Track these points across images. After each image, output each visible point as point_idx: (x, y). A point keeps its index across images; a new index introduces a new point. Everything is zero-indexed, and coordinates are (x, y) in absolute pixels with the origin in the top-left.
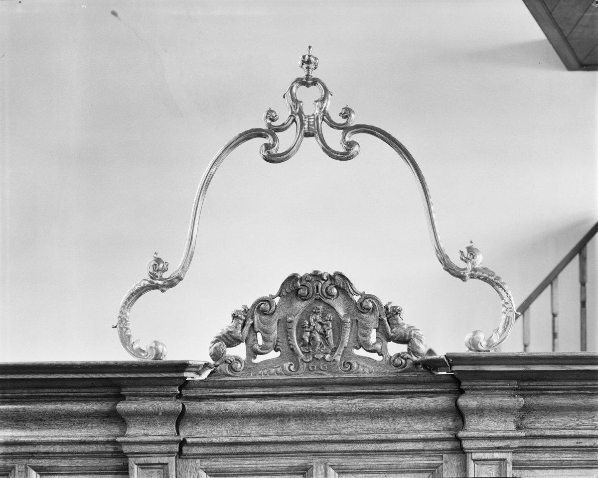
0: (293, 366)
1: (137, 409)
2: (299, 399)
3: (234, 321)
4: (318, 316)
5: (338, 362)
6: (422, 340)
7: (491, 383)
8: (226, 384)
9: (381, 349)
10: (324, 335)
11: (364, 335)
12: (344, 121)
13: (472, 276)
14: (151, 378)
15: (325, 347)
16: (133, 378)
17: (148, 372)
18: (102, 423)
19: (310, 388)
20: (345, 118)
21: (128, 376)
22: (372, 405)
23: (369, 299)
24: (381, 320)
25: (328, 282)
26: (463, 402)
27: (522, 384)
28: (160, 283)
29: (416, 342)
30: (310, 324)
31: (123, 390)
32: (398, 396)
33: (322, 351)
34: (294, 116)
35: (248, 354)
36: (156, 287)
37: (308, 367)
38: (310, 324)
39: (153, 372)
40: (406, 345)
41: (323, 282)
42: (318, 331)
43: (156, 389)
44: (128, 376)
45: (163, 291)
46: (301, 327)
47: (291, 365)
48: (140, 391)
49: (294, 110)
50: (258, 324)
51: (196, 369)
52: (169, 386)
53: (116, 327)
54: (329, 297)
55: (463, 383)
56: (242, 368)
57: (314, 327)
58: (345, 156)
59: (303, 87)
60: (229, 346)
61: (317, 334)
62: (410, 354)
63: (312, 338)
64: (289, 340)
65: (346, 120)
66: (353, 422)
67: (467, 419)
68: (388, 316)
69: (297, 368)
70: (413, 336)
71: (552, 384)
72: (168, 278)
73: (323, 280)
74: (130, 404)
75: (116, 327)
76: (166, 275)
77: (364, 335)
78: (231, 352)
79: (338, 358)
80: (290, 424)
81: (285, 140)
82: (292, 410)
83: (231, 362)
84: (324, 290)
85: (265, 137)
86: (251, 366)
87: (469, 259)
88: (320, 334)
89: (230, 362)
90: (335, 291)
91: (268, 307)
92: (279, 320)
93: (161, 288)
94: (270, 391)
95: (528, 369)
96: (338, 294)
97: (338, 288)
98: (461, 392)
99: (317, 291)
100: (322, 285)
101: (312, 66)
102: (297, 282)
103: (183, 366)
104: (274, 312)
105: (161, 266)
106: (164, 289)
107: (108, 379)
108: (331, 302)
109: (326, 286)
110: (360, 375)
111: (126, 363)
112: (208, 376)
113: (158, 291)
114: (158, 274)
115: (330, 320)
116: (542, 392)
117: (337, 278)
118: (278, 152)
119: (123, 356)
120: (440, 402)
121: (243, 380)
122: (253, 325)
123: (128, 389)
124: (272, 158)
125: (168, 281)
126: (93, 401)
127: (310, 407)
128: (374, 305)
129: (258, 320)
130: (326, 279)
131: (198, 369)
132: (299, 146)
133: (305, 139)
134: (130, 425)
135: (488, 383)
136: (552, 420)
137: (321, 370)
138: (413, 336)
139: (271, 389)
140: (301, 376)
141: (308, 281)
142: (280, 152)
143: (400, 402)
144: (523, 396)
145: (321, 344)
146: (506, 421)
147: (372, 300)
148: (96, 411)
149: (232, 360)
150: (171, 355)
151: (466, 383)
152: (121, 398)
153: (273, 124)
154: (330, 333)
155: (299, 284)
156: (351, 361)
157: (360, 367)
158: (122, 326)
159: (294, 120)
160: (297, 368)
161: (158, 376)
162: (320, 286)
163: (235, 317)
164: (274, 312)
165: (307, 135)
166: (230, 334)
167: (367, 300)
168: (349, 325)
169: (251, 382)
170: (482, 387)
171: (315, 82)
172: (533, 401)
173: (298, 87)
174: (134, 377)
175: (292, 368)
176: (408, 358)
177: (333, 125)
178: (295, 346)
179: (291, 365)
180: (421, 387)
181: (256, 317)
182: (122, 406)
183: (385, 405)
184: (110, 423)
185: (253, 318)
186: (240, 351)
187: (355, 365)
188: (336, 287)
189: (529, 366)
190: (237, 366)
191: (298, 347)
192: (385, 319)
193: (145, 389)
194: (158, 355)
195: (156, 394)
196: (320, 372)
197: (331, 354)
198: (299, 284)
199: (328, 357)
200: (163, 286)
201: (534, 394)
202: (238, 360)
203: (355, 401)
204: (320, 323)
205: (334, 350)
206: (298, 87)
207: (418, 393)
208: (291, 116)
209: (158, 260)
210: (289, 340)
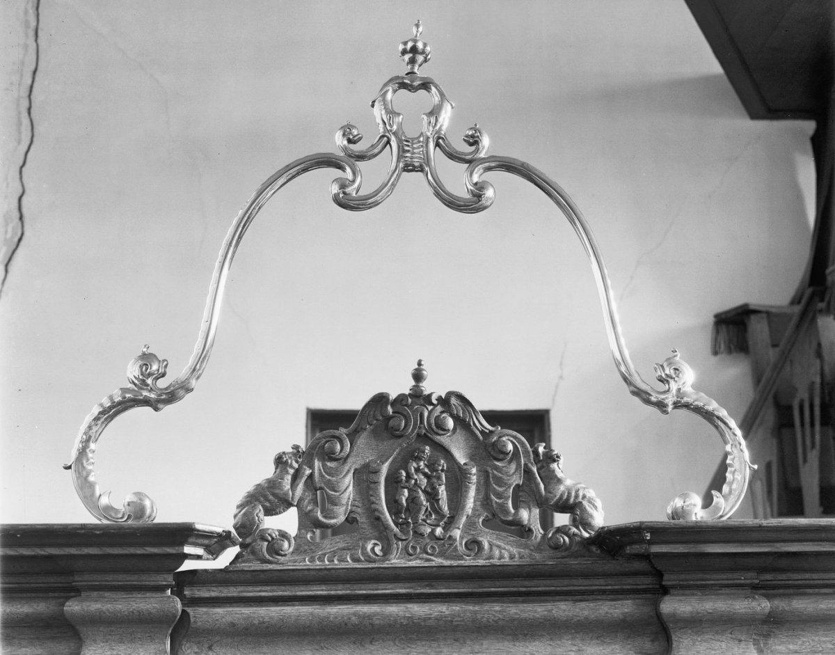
0: (380, 547)
1: (101, 612)
2: (591, 238)
3: (278, 470)
4: (422, 463)
5: (455, 540)
6: (596, 504)
7: (715, 576)
8: (262, 576)
9: (529, 520)
10: (432, 496)
11: (499, 496)
12: (467, 149)
13: (677, 405)
14: (126, 555)
15: (433, 517)
16: (95, 555)
17: (121, 545)
18: (37, 638)
19: (409, 585)
20: (471, 144)
21: (86, 551)
22: (516, 614)
23: (507, 438)
24: (528, 472)
25: (439, 408)
26: (671, 606)
27: (762, 578)
28: (153, 396)
29: (588, 508)
30: (409, 477)
31: (77, 578)
32: (557, 598)
33: (428, 521)
34: (388, 138)
35: (301, 526)
36: (146, 402)
37: (406, 548)
38: (409, 477)
39: (131, 545)
40: (568, 515)
41: (430, 408)
42: (423, 487)
43: (136, 577)
44: (86, 551)
45: (156, 409)
46: (393, 482)
47: (376, 544)
48: (108, 581)
49: (389, 128)
50: (321, 475)
51: (206, 542)
52: (159, 571)
53: (70, 467)
54: (443, 432)
55: (666, 577)
56: (291, 550)
57: (416, 480)
58: (473, 204)
59: (403, 92)
60: (269, 512)
61: (420, 492)
62: (577, 528)
63: (413, 500)
64: (373, 503)
65: (473, 148)
66: (482, 644)
67: (674, 637)
68: (539, 465)
69: (386, 551)
70: (581, 497)
71: (814, 578)
72: (166, 389)
73: (432, 404)
74: (88, 604)
75: (70, 467)
76: (162, 383)
77: (499, 496)
78: (271, 524)
79: (457, 533)
80: (372, 648)
81: (368, 177)
82: (377, 622)
83: (273, 538)
84: (433, 421)
85: (343, 169)
86: (306, 547)
87: (672, 378)
88: (425, 491)
89: (270, 538)
90: (450, 423)
91: (338, 447)
92: (356, 470)
93: (154, 405)
94: (341, 591)
95: (776, 550)
96: (455, 429)
97: (456, 418)
98: (665, 591)
99: (422, 422)
100: (430, 412)
101: (420, 58)
102: (386, 408)
103: (184, 533)
104: (348, 456)
105: (155, 367)
106: (160, 406)
107: (50, 557)
108: (444, 440)
109: (437, 413)
110: (495, 561)
111: (83, 527)
112: (230, 564)
113: (148, 409)
114: (149, 381)
115: (442, 470)
116: (799, 590)
117: (453, 401)
118: (360, 193)
119: (79, 515)
120: (623, 608)
121: (293, 570)
122: (311, 476)
123: (86, 577)
124: (345, 203)
125: (166, 394)
126: (22, 598)
127: (410, 617)
128: (515, 446)
129: (320, 470)
130: (435, 402)
131: (217, 543)
132: (394, 185)
133: (405, 174)
134: (88, 641)
135: (708, 577)
136: (817, 639)
137: (427, 553)
138: (581, 497)
139: (341, 586)
140: (396, 561)
141: (406, 405)
142: (362, 193)
143: (563, 609)
144: (768, 597)
145: (427, 509)
146: (740, 641)
147: (511, 439)
148: (27, 615)
149: (274, 535)
150: (165, 513)
151: (672, 577)
152: (73, 591)
153: (352, 146)
154: (442, 491)
155: (390, 409)
156: (480, 539)
157: (494, 548)
158: (79, 465)
159: (388, 142)
160: (386, 551)
161: (139, 551)
162: (426, 414)
163: (280, 461)
164: (348, 456)
165: (409, 168)
166: (272, 490)
167: (504, 439)
168: (474, 479)
169: (306, 573)
170: (699, 583)
171: (426, 85)
172: (781, 604)
173: (395, 91)
174: (96, 553)
175: (378, 550)
176: (575, 535)
177: (453, 156)
178: (383, 514)
179: (376, 544)
180: (597, 583)
181: (317, 464)
182: (73, 607)
183: (538, 613)
184: (53, 638)
185: (311, 467)
186: (287, 522)
187: (486, 546)
188: (452, 416)
189: (778, 545)
190: (282, 545)
191: (387, 514)
192: (535, 469)
193: (116, 576)
194: (139, 511)
195: (135, 585)
196: (425, 556)
197: (444, 528)
198: (390, 409)
199: (439, 531)
200: (159, 401)
201: (784, 595)
202: (284, 535)
203: (486, 607)
204: (425, 475)
205: (450, 523)
206: (395, 91)
207: (592, 592)
208: (383, 136)
209: (147, 358)
210: (373, 503)
